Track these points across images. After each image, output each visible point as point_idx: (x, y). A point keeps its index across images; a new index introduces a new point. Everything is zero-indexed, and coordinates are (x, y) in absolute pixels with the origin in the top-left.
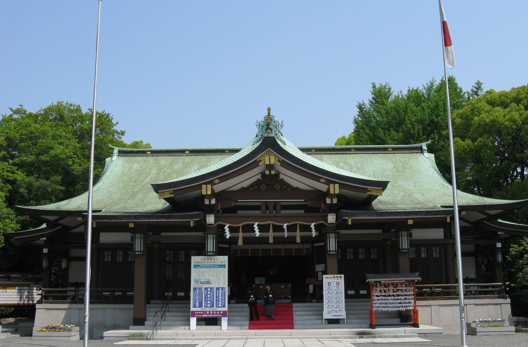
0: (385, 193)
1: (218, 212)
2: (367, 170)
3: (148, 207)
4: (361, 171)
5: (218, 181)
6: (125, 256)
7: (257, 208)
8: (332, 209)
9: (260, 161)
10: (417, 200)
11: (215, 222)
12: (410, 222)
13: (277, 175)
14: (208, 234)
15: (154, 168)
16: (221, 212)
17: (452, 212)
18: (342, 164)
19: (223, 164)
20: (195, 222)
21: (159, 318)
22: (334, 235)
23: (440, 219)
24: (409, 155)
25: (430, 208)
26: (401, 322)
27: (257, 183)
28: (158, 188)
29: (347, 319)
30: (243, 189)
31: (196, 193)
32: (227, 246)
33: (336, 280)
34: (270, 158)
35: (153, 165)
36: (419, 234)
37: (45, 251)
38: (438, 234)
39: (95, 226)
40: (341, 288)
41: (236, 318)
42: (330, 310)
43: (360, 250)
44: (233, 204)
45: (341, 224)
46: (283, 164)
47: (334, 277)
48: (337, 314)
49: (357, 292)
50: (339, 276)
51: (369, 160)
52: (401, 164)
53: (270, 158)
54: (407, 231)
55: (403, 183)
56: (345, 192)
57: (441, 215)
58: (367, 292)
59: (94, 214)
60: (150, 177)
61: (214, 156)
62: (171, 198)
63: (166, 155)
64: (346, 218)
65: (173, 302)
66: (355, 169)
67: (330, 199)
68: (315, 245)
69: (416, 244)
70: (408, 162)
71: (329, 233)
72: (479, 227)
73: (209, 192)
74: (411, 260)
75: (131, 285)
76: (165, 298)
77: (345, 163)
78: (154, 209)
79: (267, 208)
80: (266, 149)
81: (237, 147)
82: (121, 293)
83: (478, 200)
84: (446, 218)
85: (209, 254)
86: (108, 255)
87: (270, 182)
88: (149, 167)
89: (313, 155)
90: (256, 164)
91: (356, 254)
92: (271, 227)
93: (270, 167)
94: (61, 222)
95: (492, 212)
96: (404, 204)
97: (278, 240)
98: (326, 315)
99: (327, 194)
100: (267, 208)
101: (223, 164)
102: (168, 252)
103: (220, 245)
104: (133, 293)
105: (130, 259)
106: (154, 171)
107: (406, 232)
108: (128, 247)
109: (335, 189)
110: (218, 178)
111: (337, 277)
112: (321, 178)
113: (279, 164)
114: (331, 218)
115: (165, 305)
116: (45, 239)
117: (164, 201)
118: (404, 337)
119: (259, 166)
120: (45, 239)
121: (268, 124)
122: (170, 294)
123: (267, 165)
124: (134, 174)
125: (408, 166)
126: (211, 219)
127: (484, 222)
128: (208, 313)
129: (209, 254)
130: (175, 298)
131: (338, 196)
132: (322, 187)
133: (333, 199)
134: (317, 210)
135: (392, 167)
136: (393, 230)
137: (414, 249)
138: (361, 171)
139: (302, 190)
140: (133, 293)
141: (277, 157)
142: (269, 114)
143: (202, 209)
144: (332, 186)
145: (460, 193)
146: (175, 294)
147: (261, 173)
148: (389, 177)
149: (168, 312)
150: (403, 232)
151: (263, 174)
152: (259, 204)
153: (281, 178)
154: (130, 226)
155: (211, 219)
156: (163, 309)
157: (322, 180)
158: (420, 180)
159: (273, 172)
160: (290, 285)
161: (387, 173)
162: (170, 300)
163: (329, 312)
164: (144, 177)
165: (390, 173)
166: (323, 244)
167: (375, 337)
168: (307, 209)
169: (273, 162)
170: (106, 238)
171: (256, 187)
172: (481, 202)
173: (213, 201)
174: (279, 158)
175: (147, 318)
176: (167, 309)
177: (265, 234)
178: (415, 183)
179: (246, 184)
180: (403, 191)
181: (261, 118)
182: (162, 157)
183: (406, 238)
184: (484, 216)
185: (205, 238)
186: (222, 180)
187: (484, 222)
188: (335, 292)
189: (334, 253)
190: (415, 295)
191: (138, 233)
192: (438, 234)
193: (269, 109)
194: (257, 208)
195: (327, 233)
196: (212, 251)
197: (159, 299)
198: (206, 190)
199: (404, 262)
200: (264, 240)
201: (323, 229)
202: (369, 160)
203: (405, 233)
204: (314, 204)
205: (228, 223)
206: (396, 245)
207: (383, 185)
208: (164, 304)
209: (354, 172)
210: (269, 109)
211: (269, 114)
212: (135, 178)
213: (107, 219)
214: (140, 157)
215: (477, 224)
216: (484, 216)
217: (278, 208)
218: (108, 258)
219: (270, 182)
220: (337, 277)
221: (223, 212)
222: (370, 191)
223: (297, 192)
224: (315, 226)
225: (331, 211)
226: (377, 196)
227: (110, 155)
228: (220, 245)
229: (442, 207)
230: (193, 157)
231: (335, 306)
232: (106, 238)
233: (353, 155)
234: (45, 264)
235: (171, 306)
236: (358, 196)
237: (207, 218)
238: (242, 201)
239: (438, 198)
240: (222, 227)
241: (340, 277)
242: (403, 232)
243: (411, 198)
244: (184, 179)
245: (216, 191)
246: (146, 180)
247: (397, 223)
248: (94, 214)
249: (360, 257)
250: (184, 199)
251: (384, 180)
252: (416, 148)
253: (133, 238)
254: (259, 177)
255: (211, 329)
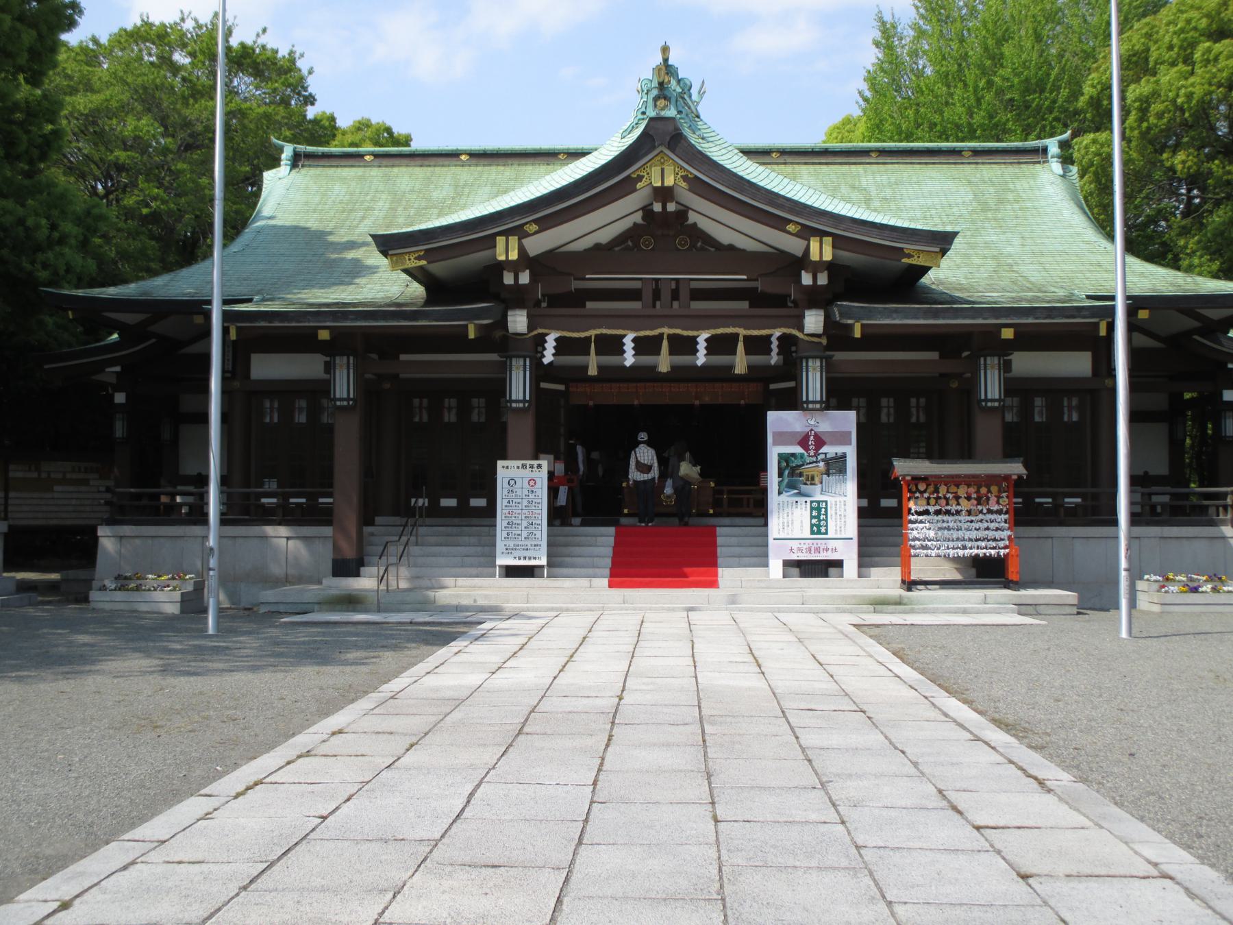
0: (945, 262)
1: (538, 304)
2: (908, 204)
3: (365, 290)
4: (893, 207)
5: (534, 227)
6: (314, 411)
7: (634, 295)
8: (815, 298)
9: (640, 178)
10: (1029, 281)
11: (531, 327)
12: (1008, 334)
13: (682, 213)
14: (511, 358)
15: (384, 196)
16: (544, 305)
17: (1111, 311)
18: (844, 189)
19: (547, 185)
20: (479, 328)
21: (393, 560)
22: (818, 363)
23: (1079, 328)
24: (1011, 169)
25: (1059, 301)
26: (978, 576)
27: (630, 236)
28: (388, 244)
29: (550, 565)
30: (598, 247)
31: (477, 258)
32: (561, 387)
33: (527, 473)
34: (663, 170)
35: (381, 188)
36: (1027, 363)
37: (120, 398)
38: (1078, 364)
39: (233, 335)
40: (539, 492)
41: (442, 560)
42: (511, 544)
43: (884, 402)
44: (575, 285)
45: (836, 336)
46: (697, 186)
47: (524, 467)
48: (527, 554)
49: (463, 502)
50: (535, 463)
51: (914, 179)
52: (992, 190)
53: (664, 173)
54: (999, 356)
55: (994, 238)
56: (847, 256)
57: (1084, 317)
58: (488, 502)
59: (227, 308)
60: (372, 218)
61: (530, 168)
62: (421, 267)
63: (412, 163)
64: (850, 322)
65: (428, 521)
66: (876, 203)
67: (512, 275)
68: (773, 386)
69: (1016, 388)
70: (1011, 186)
71: (807, 358)
72: (1175, 342)
73: (513, 255)
74: (1008, 428)
75: (326, 482)
76: (408, 512)
77: (853, 187)
78: (380, 295)
79: (657, 295)
80: (654, 148)
81: (585, 146)
82: (304, 500)
83: (1181, 282)
84: (1097, 325)
85: (811, 406)
86: (272, 408)
87: (664, 228)
88: (372, 193)
89: (775, 167)
90: (627, 186)
91: (464, 411)
92: (665, 343)
93: (664, 194)
94: (158, 328)
95: (1215, 314)
96: (995, 290)
97: (681, 375)
98: (503, 561)
99: (802, 262)
100: (675, 295)
101: (547, 185)
102: (416, 401)
103: (543, 385)
104: (330, 500)
105: (325, 419)
106: (383, 204)
107: (996, 360)
108: (318, 391)
109: (821, 250)
110: (535, 221)
111: (532, 466)
112: (790, 221)
113: (684, 184)
114: (813, 321)
115: (409, 529)
116: (118, 369)
117: (404, 276)
118: (978, 612)
119: (635, 190)
120: (118, 369)
121: (666, 84)
122: (420, 502)
123: (656, 189)
124: (332, 212)
125: (1010, 196)
126: (518, 321)
127: (1196, 337)
128: (814, 521)
129: (811, 406)
130: (464, 513)
131: (831, 267)
132: (791, 244)
133: (819, 275)
134: (779, 301)
135: (971, 196)
136: (966, 354)
137: (1016, 401)
138: (893, 207)
139: (744, 250)
140: (330, 500)
141: (682, 168)
142: (666, 60)
143: (495, 297)
144: (814, 245)
145: (1134, 262)
146: (434, 503)
147: (643, 209)
148: (962, 221)
149: (417, 544)
150: (988, 359)
151: (647, 211)
152: (638, 285)
153: (691, 221)
154: (1003, 337)
155: (518, 321)
156: (404, 539)
157: (791, 228)
158: (1039, 231)
159: (671, 207)
160: (712, 484)
161: (958, 214)
162: (421, 516)
163: (508, 551)
164: (358, 219)
165: (965, 212)
166: (792, 384)
167: (912, 612)
168: (757, 299)
169: (669, 182)
170: (266, 367)
171: (630, 243)
172: (1187, 287)
173: (525, 278)
174: (685, 170)
175: (366, 559)
176: (413, 539)
177: (647, 360)
178: (1028, 237)
179: (604, 237)
180: (994, 258)
181: (646, 68)
182: (403, 169)
183: (996, 372)
184: (1196, 324)
185: (504, 368)
186: (546, 223)
187: (1196, 337)
188: (525, 503)
189: (996, 404)
190: (1012, 512)
191: (342, 355)
192: (1078, 364)
193: (665, 50)
194: (634, 295)
195: (801, 358)
196: (521, 398)
197: (396, 513)
198: (507, 250)
199: (988, 431)
200: (642, 374)
201: (794, 349)
202: (914, 179)
203: (993, 361)
204: (772, 284)
205: (557, 329)
206: (970, 389)
207: (942, 241)
208: (405, 526)
209: (875, 211)
210: (665, 50)
211: (666, 60)
212: (335, 220)
213: (1006, 316)
214: (347, 169)
215: (1177, 343)
216: (1196, 324)
217: (684, 294)
218: (272, 417)
219: (664, 228)
220: (532, 466)
221: (549, 306)
222: (909, 256)
223: (730, 256)
224: (556, 340)
225: (813, 305)
226: (929, 268)
227: (274, 162)
228: (543, 385)
229: (1089, 297)
230: (479, 168)
231: (525, 534)
232: (266, 367)
233: (875, 167)
234: (120, 430)
235: (422, 530)
236: (883, 269)
237: (509, 319)
238: (596, 280)
239: (1080, 276)
240: (540, 341)
241: (539, 466)
242: (988, 359)
243: (1014, 276)
244: (451, 221)
245: (532, 252)
246: (362, 225)
247: (976, 337)
248: (227, 308)
249: (475, 417)
250: (459, 269)
251: (949, 229)
252: (1034, 151)
253: (329, 368)
254: (638, 218)
255: (815, 586)
